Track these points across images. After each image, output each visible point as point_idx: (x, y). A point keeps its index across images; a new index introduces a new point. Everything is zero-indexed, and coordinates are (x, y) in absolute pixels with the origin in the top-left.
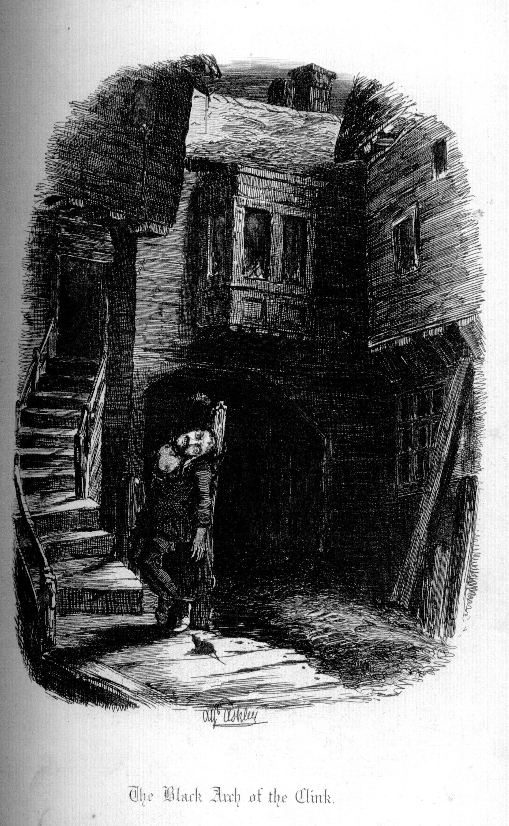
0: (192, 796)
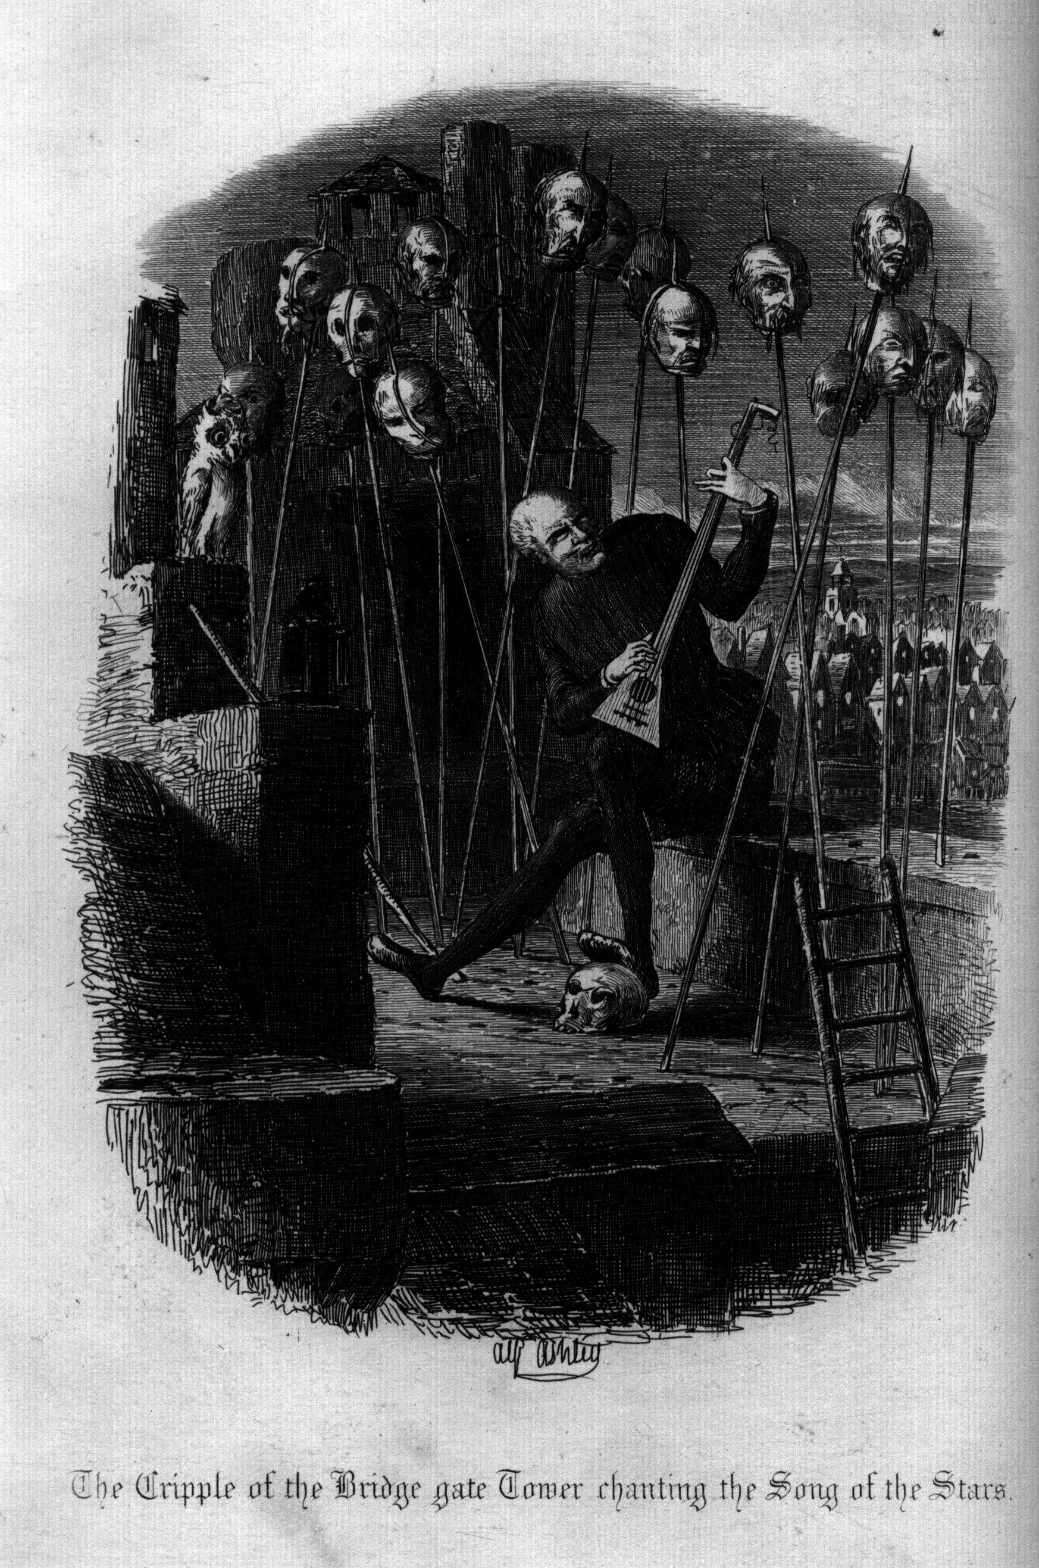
0: (604, 1488)
